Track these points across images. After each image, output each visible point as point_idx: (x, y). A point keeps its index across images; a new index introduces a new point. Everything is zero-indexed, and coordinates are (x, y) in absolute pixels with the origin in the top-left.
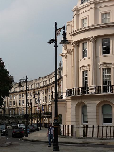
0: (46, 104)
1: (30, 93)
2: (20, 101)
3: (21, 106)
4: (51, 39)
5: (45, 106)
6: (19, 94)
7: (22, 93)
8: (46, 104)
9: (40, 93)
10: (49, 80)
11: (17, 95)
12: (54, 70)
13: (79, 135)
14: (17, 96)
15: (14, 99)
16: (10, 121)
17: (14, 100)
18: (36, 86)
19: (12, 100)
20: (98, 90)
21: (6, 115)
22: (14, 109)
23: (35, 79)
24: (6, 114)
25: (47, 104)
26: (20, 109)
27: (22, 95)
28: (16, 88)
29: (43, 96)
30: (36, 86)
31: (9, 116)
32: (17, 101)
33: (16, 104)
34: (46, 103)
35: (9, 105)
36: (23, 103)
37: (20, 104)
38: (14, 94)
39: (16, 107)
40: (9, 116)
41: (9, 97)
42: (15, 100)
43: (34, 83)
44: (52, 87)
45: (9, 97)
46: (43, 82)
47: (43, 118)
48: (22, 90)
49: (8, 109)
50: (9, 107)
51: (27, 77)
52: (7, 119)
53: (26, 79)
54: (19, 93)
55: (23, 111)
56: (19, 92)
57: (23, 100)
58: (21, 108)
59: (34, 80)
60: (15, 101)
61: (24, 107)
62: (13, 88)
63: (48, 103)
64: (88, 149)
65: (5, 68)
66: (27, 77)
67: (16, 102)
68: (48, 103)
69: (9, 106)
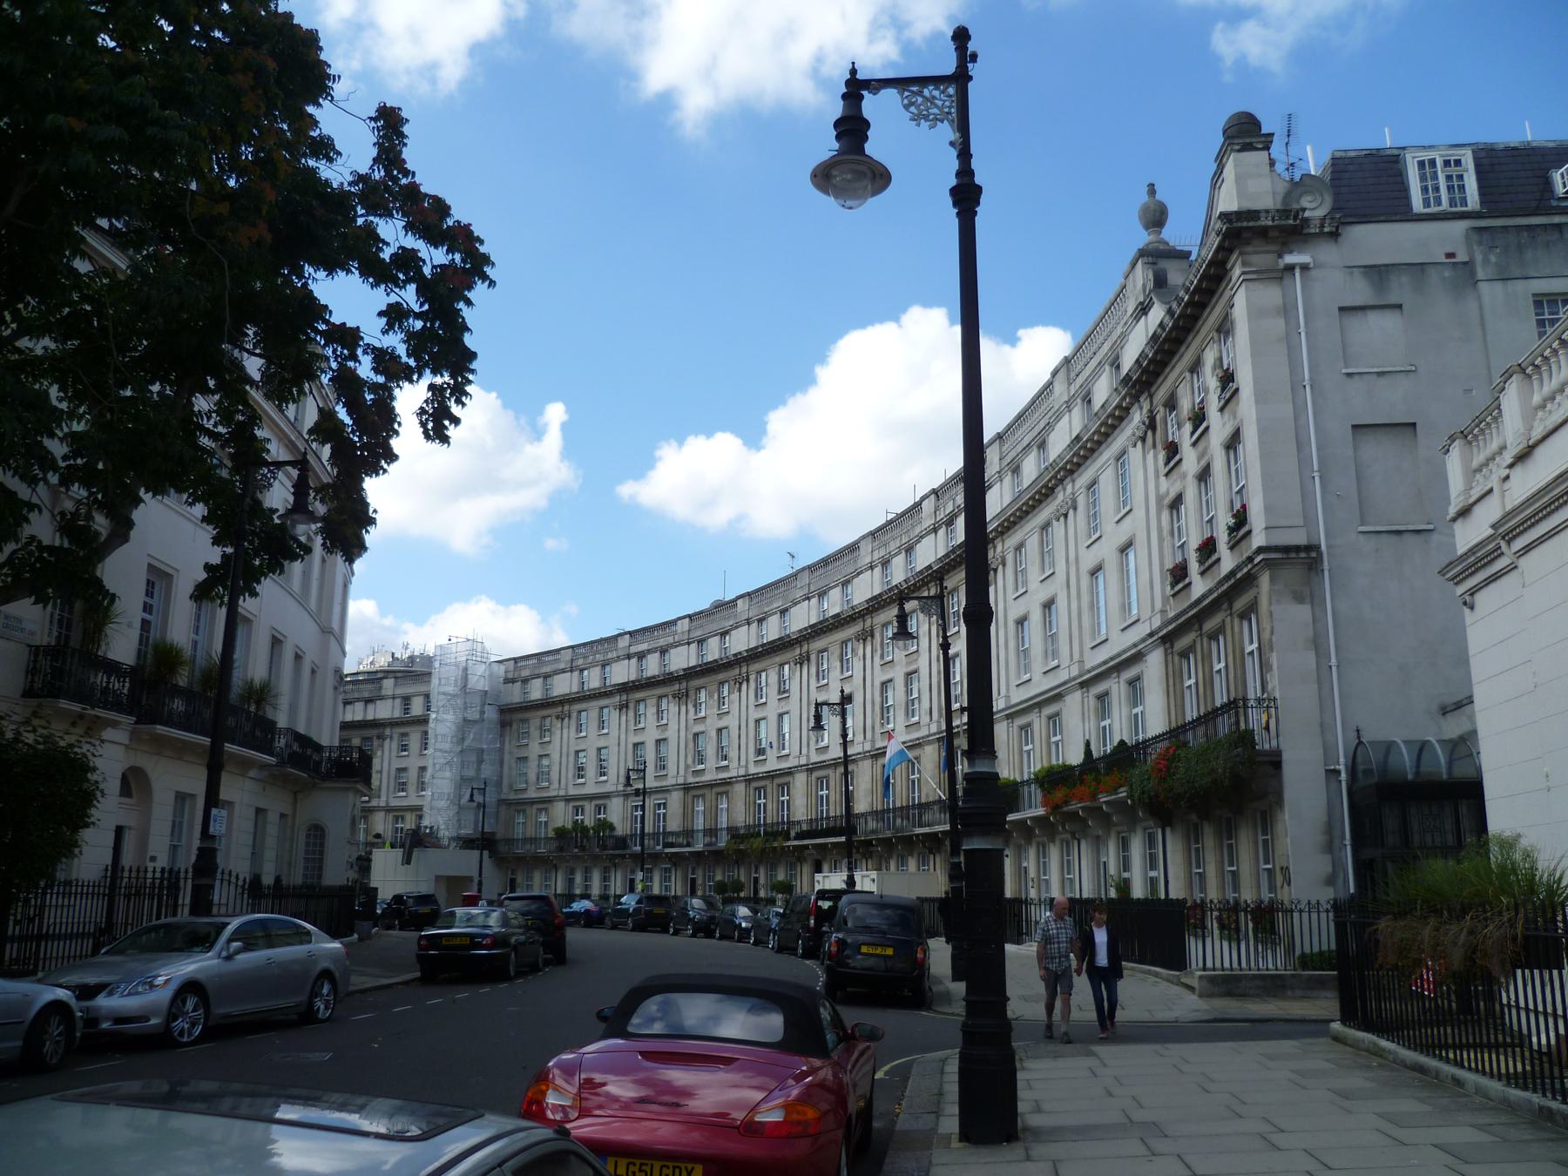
1: (837, 652)
3: (591, 789)
6: (759, 673)
7: (778, 659)
11: (739, 682)
12: (954, 461)
13: (1527, 1010)
14: (744, 686)
18: (700, 655)
19: (709, 721)
21: (672, 833)
23: (873, 528)
24: (668, 830)
26: (762, 783)
27: (652, 711)
35: (690, 761)
38: (721, 676)
39: (733, 773)
42: (731, 721)
43: (868, 560)
45: (690, 707)
46: (760, 621)
48: (717, 656)
49: (681, 793)
50: (691, 780)
55: (786, 798)
56: (690, 674)
58: (771, 776)
59: (864, 537)
61: (607, 796)
62: (717, 638)
63: (873, 741)
64: (186, 879)
68: (873, 741)
69: (687, 767)
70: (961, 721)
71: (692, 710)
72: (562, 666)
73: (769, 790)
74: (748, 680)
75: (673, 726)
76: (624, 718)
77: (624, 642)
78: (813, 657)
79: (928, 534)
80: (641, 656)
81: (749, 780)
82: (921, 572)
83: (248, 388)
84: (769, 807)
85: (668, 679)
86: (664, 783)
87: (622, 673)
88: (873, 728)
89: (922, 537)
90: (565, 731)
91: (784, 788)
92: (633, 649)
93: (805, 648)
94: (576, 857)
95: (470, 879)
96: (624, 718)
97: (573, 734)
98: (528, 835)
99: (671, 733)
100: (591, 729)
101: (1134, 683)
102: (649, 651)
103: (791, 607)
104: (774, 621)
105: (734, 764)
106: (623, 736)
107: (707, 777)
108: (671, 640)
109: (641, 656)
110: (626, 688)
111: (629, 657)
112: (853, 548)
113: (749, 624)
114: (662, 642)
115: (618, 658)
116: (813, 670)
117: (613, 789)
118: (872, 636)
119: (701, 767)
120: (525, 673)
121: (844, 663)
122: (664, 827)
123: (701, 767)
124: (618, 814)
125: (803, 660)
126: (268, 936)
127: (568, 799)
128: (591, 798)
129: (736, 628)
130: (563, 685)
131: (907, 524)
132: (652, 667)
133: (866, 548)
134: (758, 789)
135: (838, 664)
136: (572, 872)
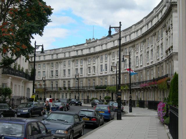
0: (142, 68)
2: (102, 65)
3: (104, 74)
4: (40, 36)
5: (140, 72)
8: (142, 68)
9: (132, 51)
10: (147, 26)
11: (98, 57)
14: (98, 58)
15: (94, 64)
16: (88, 96)
17: (94, 65)
18: (52, 57)
19: (91, 65)
20: (155, 43)
22: (94, 78)
25: (144, 66)
26: (101, 78)
28: (96, 47)
29: (136, 55)
30: (52, 57)
31: (87, 89)
32: (98, 66)
33: (96, 71)
34: (141, 66)
36: (106, 69)
37: (102, 71)
38: (94, 56)
40: (87, 89)
41: (87, 61)
44: (151, 36)
45: (87, 61)
47: (137, 92)
48: (178, 31)
51: (120, 23)
52: (84, 93)
53: (119, 26)
54: (101, 54)
56: (100, 52)
57: (106, 65)
58: (104, 76)
60: (90, 67)
61: (70, 79)
65: (22, 55)
66: (120, 23)
67: (96, 67)
69: (87, 74)
70: (118, 72)
71: (88, 62)
72: (60, 52)
73: (103, 79)
74: (99, 57)
75: (84, 65)
76: (73, 63)
77: (73, 47)
78: (112, 53)
79: (133, 33)
80: (77, 51)
81: (99, 77)
82: (143, 34)
83: (11, 18)
84: (103, 82)
85: (83, 56)
86: (82, 77)
87: (73, 54)
88: (123, 68)
89: (132, 33)
90: (61, 65)
91: (106, 79)
92: (75, 49)
93: (110, 52)
94: (64, 91)
95: (85, 128)
96: (73, 63)
97: (63, 66)
98: (91, 86)
99: (83, 67)
100: (67, 65)
101: (162, 66)
102: (79, 50)
103: (108, 43)
104: (104, 46)
105: (96, 74)
106: (73, 67)
107: (91, 76)
108: (83, 48)
109: (77, 51)
110: (74, 57)
111: (74, 51)
112: (131, 27)
113: (99, 46)
114: (81, 48)
115: (72, 51)
116: (112, 56)
117: (71, 78)
118: (123, 51)
119: (107, 72)
120: (52, 53)
121: (106, 58)
122: (82, 85)
123: (107, 72)
124: (48, 84)
125: (110, 54)
126: (167, 15)
127: (62, 79)
128: (67, 79)
129: (97, 46)
130: (61, 56)
131: (130, 30)
132: (80, 53)
133: (144, 21)
134: (113, 77)
135: (116, 55)
136: (63, 94)
